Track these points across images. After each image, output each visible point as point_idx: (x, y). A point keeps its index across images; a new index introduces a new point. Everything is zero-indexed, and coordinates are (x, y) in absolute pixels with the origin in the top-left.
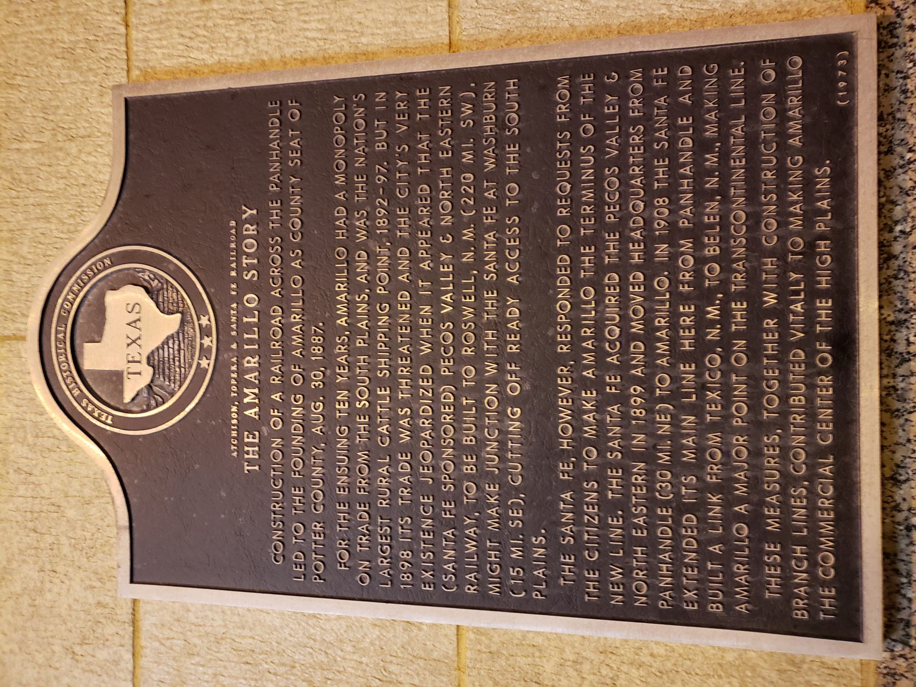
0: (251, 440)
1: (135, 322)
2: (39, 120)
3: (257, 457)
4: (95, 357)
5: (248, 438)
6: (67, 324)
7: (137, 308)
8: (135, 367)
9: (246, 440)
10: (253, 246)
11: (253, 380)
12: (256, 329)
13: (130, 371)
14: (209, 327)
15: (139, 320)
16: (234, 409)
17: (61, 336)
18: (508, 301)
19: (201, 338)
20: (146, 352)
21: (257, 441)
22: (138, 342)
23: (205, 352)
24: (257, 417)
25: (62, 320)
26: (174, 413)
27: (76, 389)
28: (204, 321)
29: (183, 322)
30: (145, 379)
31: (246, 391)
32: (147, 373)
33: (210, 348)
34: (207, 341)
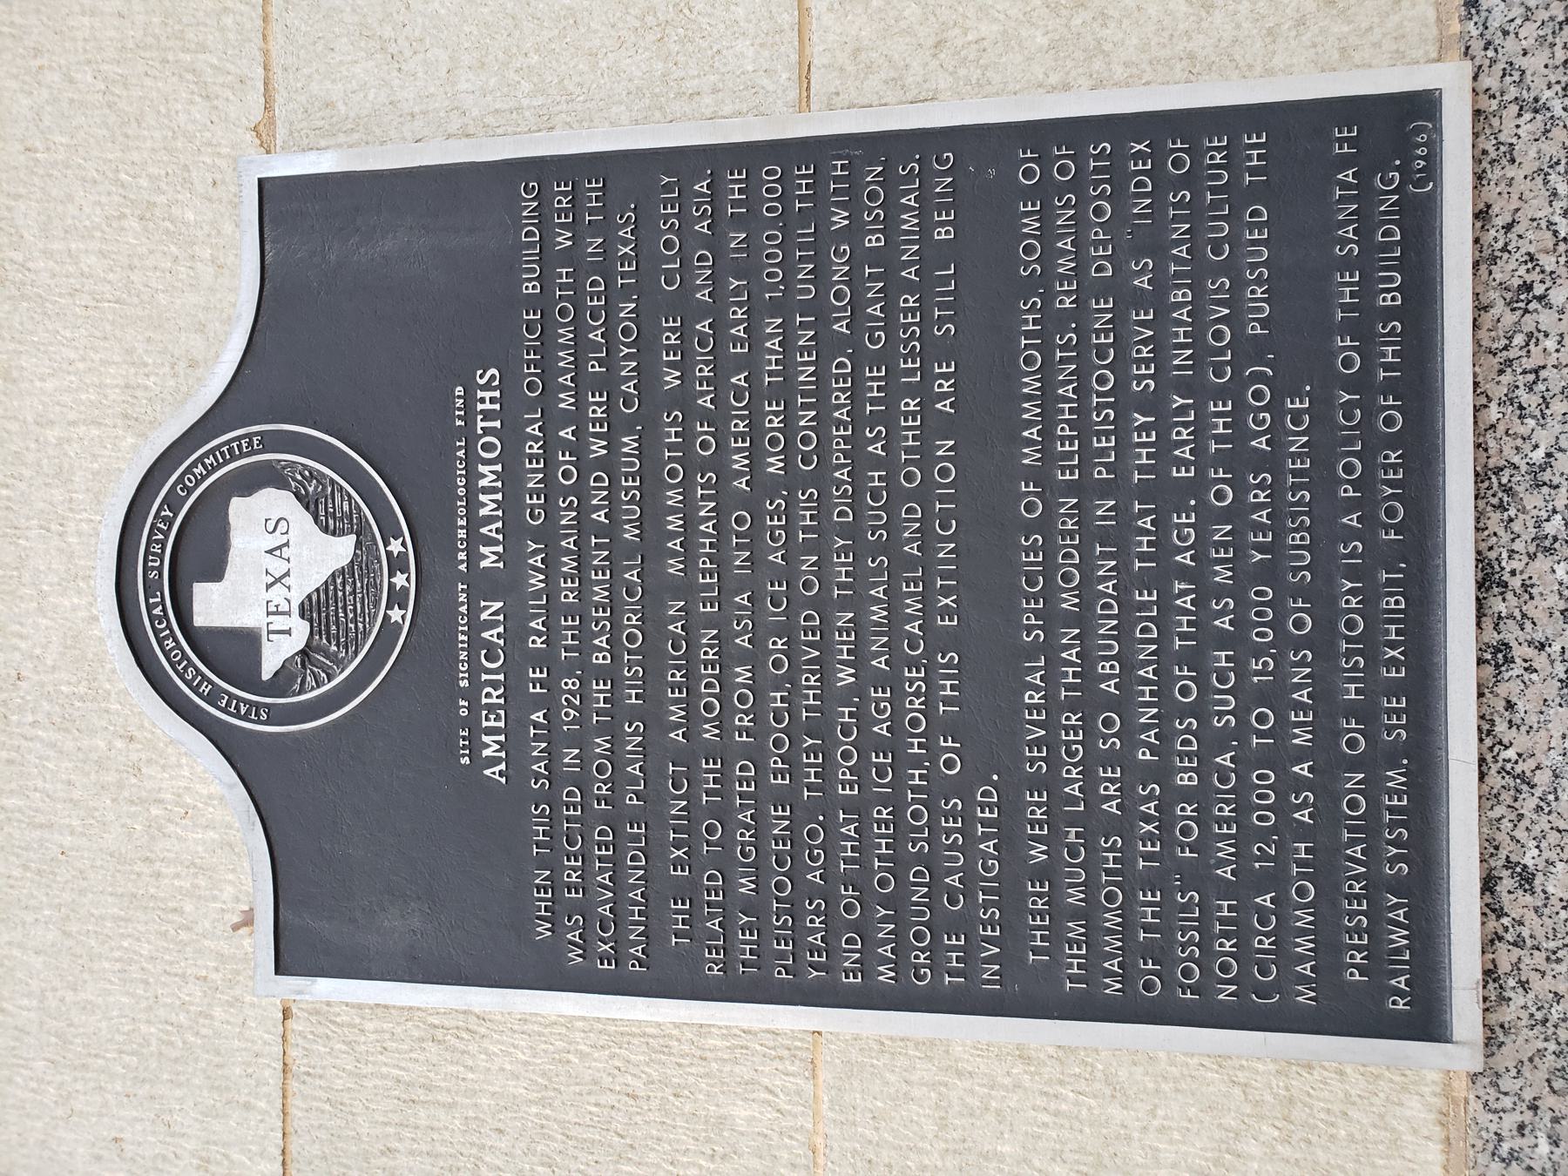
0: (492, 724)
1: (280, 548)
2: (116, 198)
3: (497, 407)
4: (212, 606)
5: (487, 719)
6: (169, 541)
7: (283, 526)
8: (279, 623)
9: (485, 724)
10: (493, 447)
11: (493, 534)
12: (502, 712)
13: (272, 627)
14: (403, 556)
15: (287, 544)
16: (459, 391)
17: (157, 611)
18: (1253, 556)
19: (389, 607)
20: (297, 598)
21: (502, 724)
22: (286, 581)
23: (397, 598)
24: (503, 780)
25: (172, 502)
26: (343, 693)
27: (191, 666)
28: (395, 547)
29: (358, 545)
30: (298, 640)
31: (483, 550)
32: (301, 631)
33: (405, 590)
34: (400, 580)
